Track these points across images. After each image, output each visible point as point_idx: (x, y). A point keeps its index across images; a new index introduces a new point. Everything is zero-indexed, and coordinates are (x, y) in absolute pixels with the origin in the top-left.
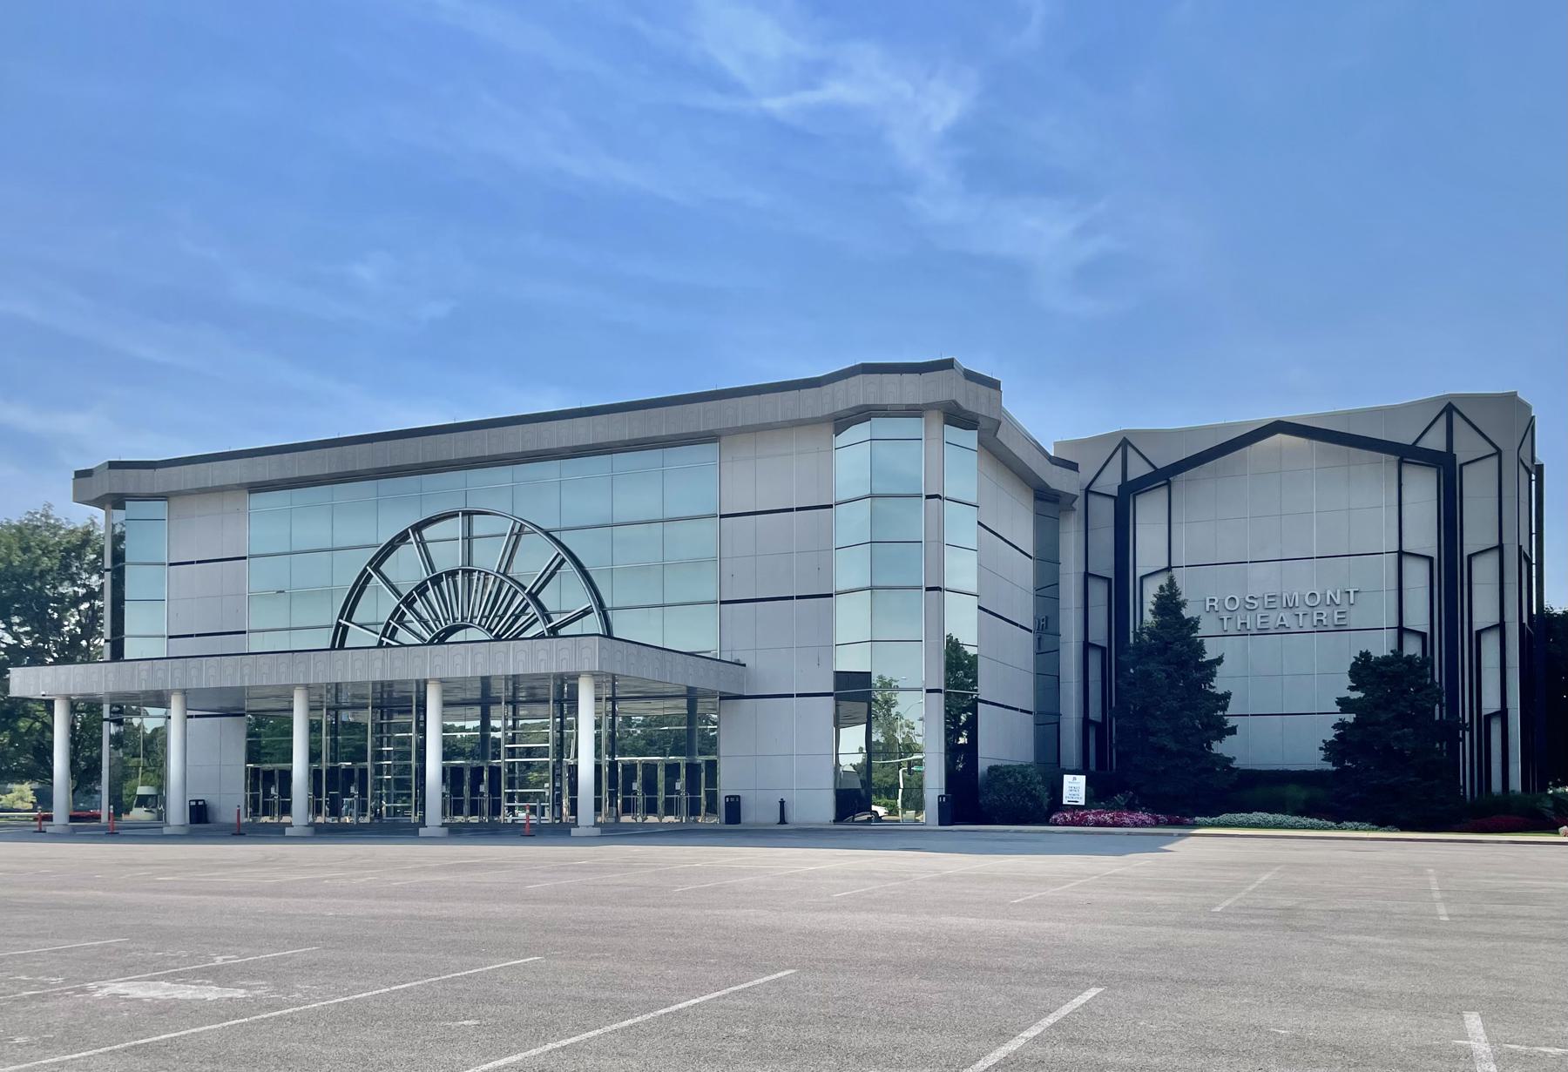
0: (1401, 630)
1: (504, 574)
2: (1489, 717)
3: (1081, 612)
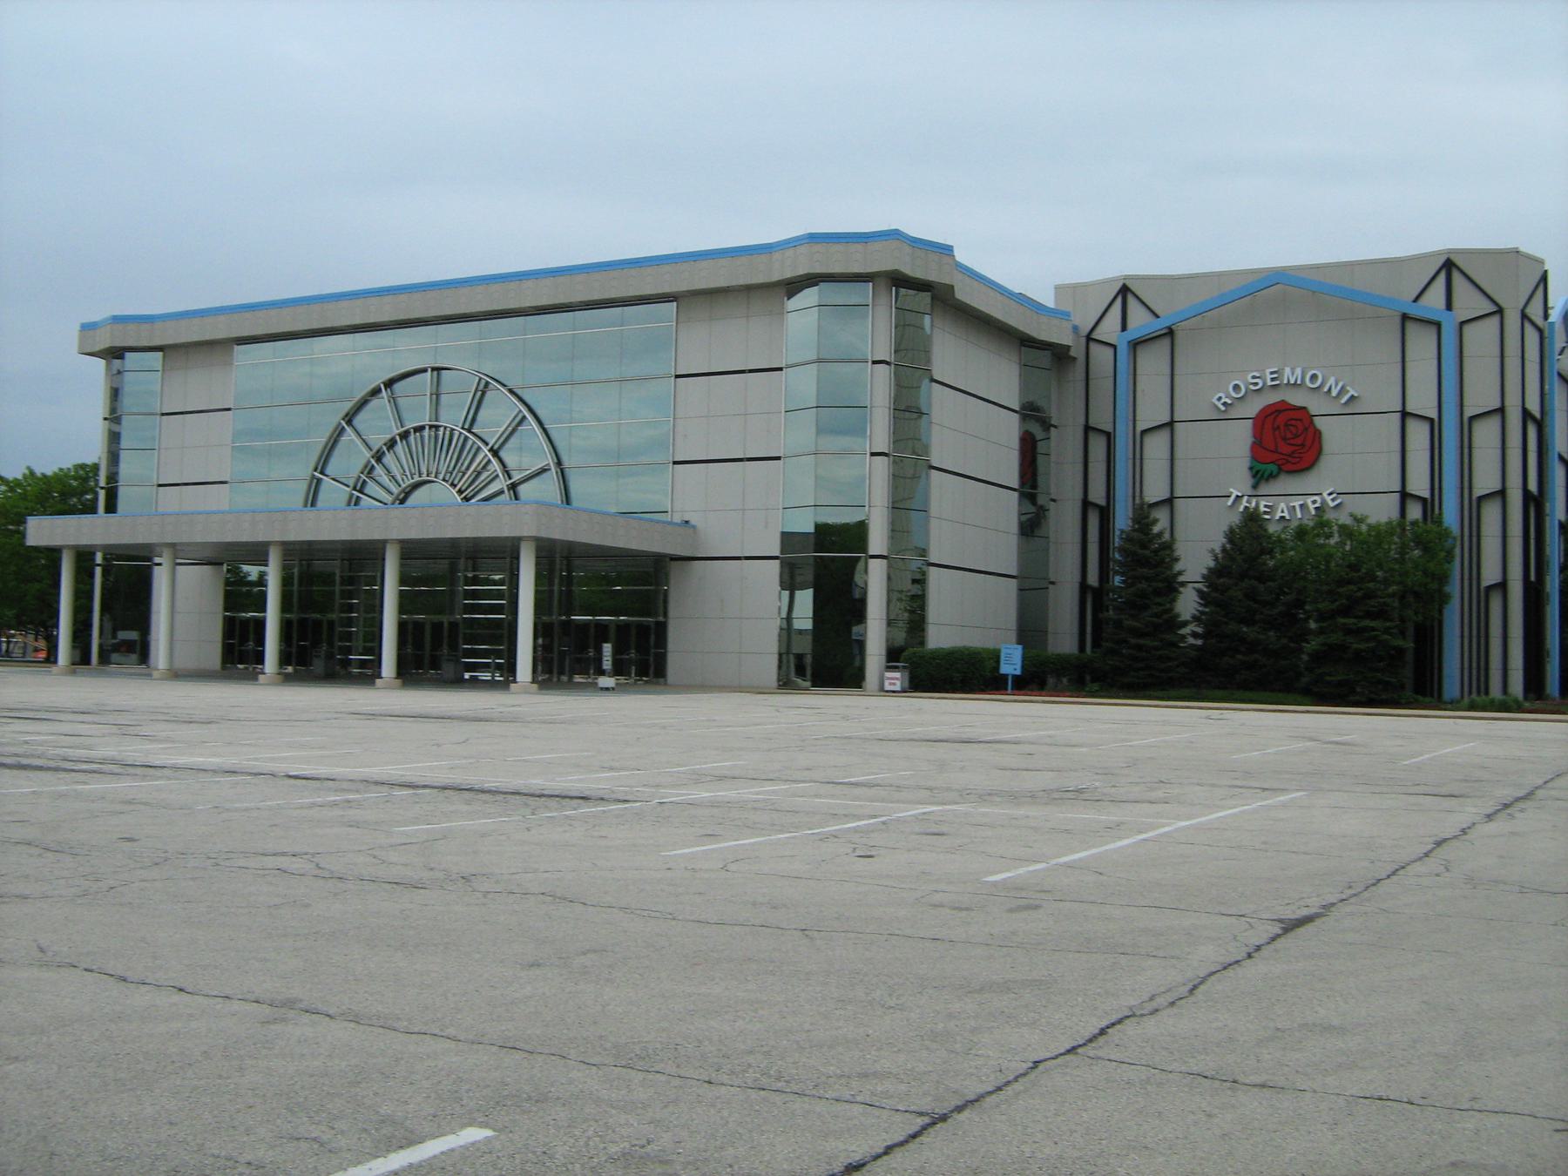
0: (1405, 496)
1: (469, 431)
2: (1489, 588)
3: (1079, 467)
